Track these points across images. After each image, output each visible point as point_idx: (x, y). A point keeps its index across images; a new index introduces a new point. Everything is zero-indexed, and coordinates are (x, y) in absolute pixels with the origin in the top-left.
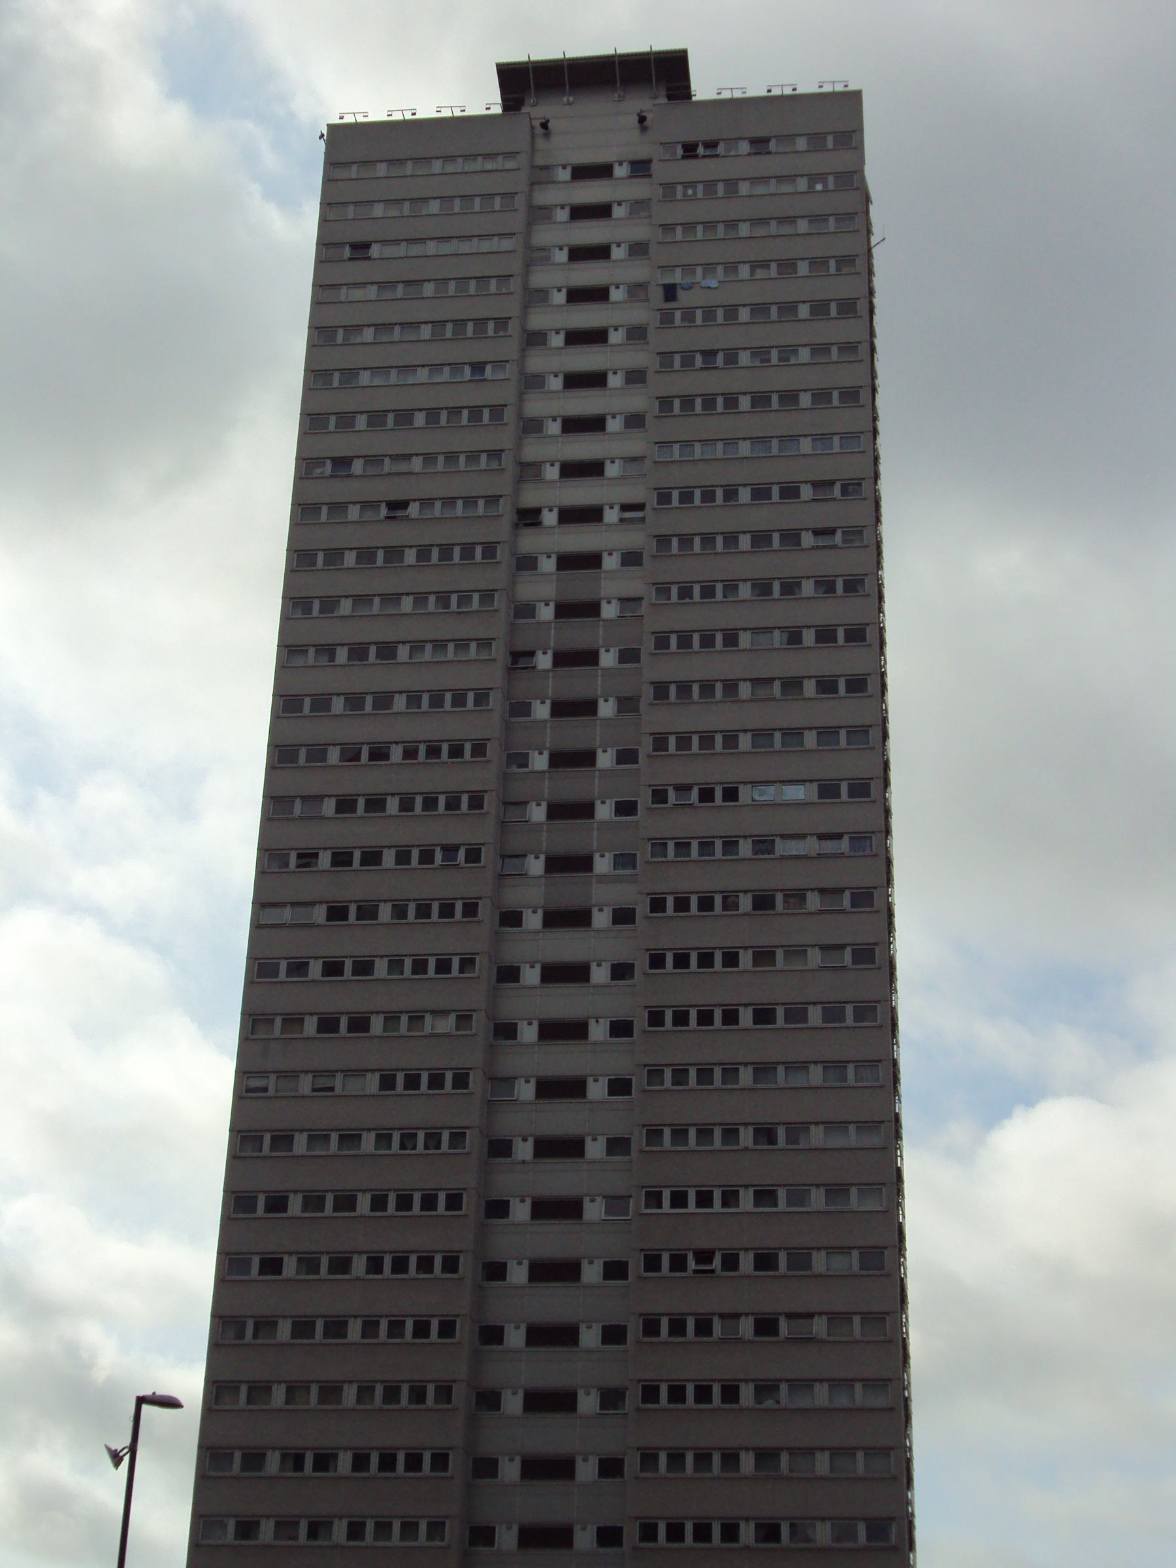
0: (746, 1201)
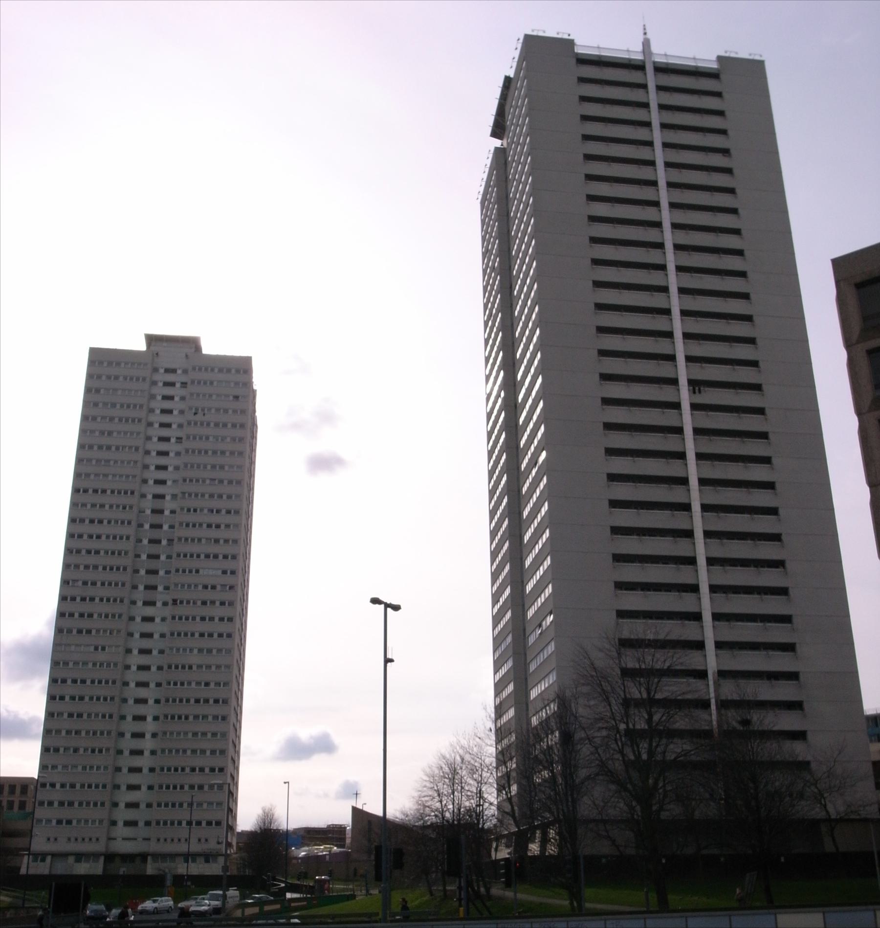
0: (193, 684)
